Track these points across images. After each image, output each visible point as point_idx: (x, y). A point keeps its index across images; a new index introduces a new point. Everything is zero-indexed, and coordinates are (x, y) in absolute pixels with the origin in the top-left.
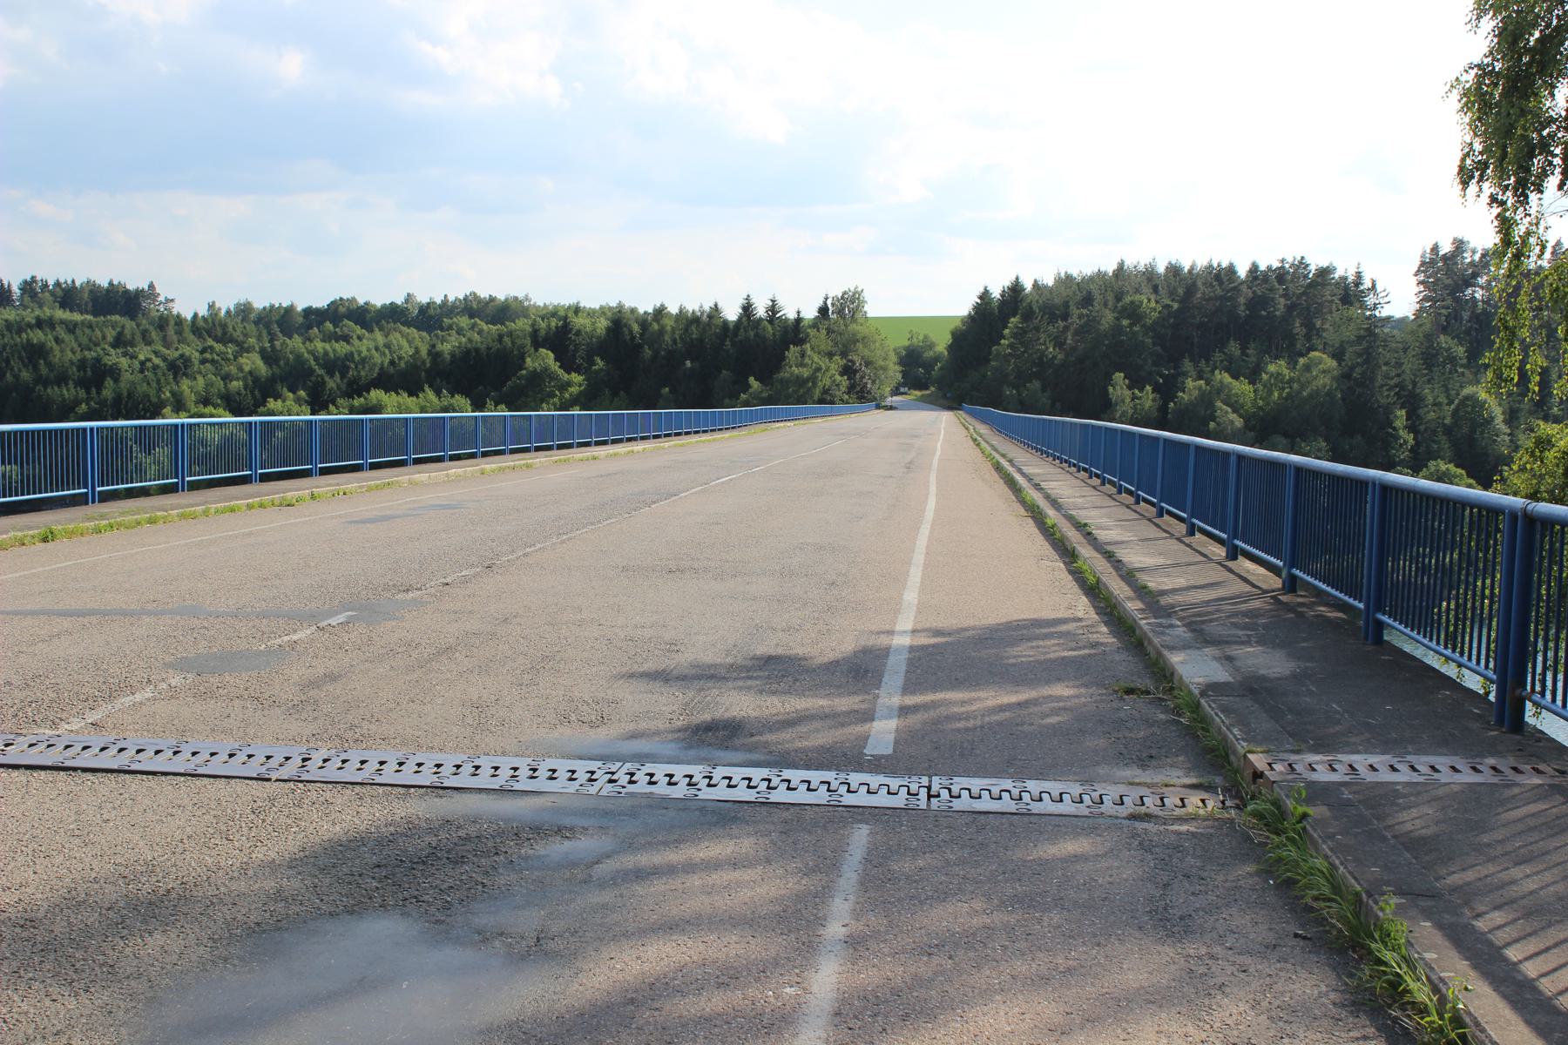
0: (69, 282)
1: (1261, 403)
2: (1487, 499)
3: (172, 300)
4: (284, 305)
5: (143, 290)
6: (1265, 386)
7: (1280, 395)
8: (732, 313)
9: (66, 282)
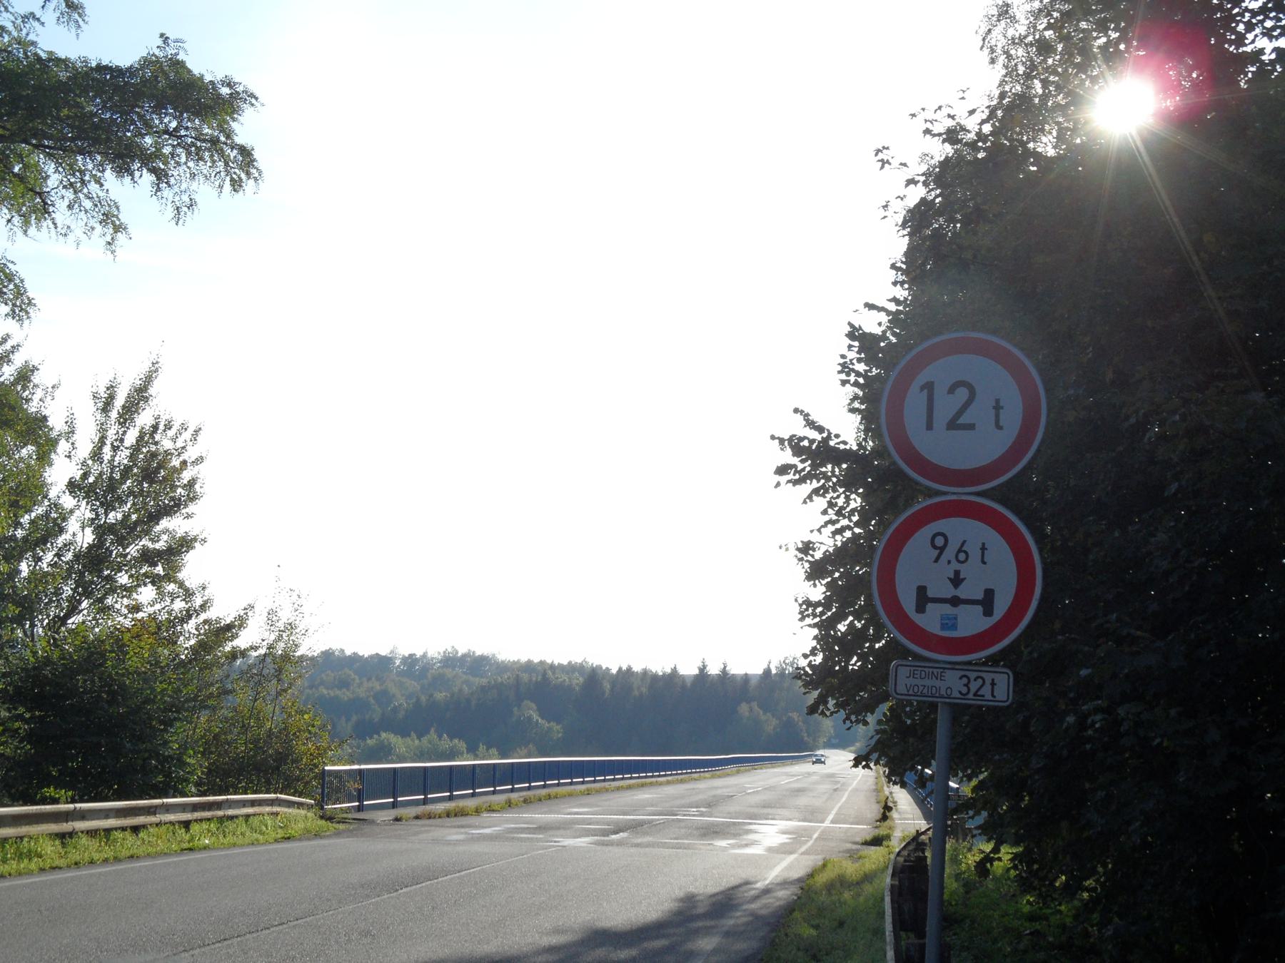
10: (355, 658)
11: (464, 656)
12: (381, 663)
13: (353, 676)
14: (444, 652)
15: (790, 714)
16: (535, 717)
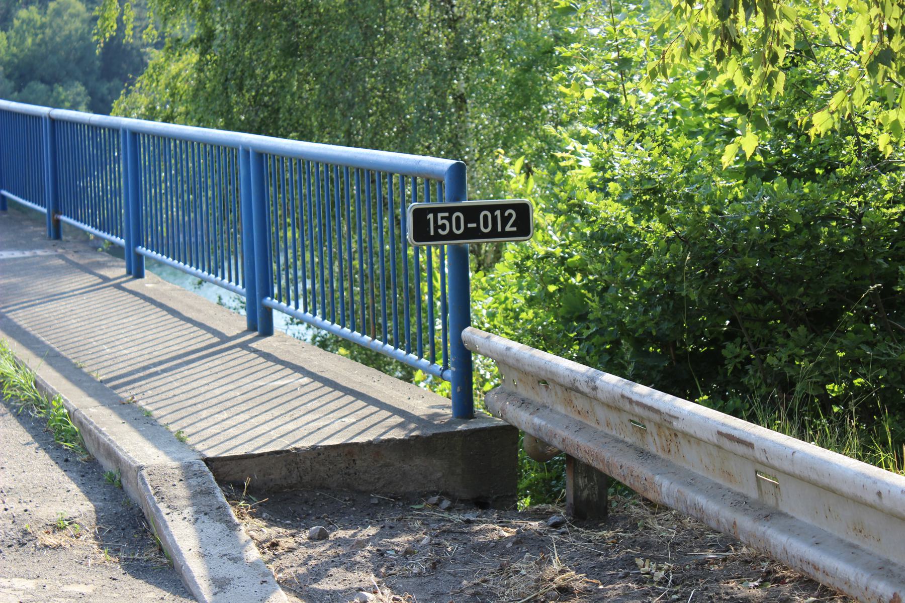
1: (14, 50)
2: (402, 162)
6: (17, 32)
7: (33, 41)
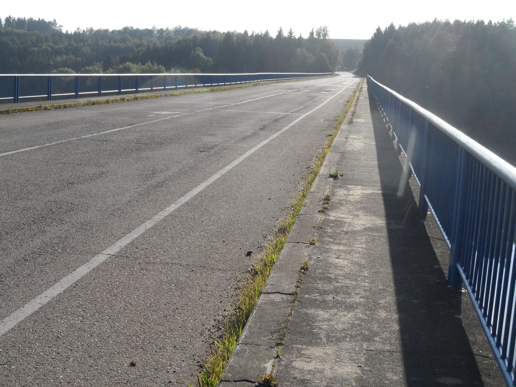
0: (23, 18)
3: (62, 26)
4: (105, 29)
5: (51, 22)
8: (274, 35)
9: (22, 18)
10: (138, 30)
11: (184, 29)
12: (148, 32)
13: (129, 37)
14: (176, 28)
15: (322, 54)
16: (201, 55)
